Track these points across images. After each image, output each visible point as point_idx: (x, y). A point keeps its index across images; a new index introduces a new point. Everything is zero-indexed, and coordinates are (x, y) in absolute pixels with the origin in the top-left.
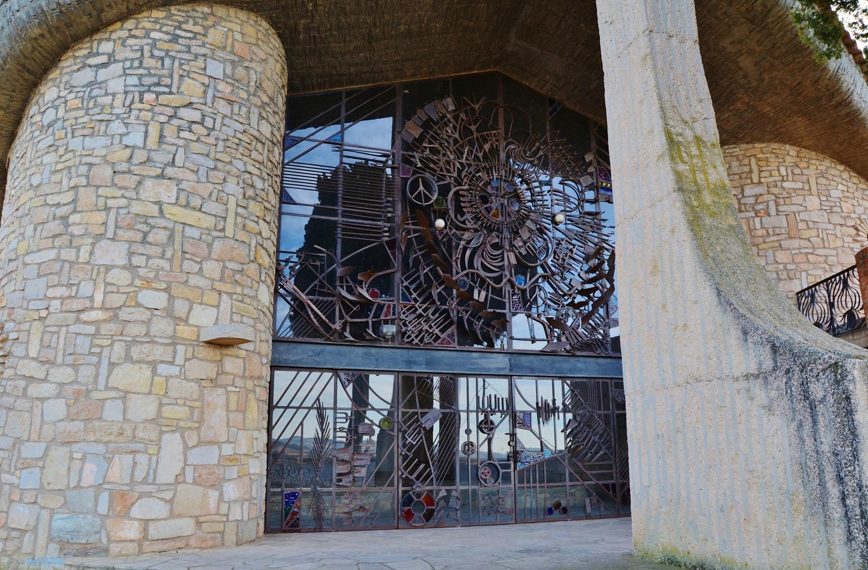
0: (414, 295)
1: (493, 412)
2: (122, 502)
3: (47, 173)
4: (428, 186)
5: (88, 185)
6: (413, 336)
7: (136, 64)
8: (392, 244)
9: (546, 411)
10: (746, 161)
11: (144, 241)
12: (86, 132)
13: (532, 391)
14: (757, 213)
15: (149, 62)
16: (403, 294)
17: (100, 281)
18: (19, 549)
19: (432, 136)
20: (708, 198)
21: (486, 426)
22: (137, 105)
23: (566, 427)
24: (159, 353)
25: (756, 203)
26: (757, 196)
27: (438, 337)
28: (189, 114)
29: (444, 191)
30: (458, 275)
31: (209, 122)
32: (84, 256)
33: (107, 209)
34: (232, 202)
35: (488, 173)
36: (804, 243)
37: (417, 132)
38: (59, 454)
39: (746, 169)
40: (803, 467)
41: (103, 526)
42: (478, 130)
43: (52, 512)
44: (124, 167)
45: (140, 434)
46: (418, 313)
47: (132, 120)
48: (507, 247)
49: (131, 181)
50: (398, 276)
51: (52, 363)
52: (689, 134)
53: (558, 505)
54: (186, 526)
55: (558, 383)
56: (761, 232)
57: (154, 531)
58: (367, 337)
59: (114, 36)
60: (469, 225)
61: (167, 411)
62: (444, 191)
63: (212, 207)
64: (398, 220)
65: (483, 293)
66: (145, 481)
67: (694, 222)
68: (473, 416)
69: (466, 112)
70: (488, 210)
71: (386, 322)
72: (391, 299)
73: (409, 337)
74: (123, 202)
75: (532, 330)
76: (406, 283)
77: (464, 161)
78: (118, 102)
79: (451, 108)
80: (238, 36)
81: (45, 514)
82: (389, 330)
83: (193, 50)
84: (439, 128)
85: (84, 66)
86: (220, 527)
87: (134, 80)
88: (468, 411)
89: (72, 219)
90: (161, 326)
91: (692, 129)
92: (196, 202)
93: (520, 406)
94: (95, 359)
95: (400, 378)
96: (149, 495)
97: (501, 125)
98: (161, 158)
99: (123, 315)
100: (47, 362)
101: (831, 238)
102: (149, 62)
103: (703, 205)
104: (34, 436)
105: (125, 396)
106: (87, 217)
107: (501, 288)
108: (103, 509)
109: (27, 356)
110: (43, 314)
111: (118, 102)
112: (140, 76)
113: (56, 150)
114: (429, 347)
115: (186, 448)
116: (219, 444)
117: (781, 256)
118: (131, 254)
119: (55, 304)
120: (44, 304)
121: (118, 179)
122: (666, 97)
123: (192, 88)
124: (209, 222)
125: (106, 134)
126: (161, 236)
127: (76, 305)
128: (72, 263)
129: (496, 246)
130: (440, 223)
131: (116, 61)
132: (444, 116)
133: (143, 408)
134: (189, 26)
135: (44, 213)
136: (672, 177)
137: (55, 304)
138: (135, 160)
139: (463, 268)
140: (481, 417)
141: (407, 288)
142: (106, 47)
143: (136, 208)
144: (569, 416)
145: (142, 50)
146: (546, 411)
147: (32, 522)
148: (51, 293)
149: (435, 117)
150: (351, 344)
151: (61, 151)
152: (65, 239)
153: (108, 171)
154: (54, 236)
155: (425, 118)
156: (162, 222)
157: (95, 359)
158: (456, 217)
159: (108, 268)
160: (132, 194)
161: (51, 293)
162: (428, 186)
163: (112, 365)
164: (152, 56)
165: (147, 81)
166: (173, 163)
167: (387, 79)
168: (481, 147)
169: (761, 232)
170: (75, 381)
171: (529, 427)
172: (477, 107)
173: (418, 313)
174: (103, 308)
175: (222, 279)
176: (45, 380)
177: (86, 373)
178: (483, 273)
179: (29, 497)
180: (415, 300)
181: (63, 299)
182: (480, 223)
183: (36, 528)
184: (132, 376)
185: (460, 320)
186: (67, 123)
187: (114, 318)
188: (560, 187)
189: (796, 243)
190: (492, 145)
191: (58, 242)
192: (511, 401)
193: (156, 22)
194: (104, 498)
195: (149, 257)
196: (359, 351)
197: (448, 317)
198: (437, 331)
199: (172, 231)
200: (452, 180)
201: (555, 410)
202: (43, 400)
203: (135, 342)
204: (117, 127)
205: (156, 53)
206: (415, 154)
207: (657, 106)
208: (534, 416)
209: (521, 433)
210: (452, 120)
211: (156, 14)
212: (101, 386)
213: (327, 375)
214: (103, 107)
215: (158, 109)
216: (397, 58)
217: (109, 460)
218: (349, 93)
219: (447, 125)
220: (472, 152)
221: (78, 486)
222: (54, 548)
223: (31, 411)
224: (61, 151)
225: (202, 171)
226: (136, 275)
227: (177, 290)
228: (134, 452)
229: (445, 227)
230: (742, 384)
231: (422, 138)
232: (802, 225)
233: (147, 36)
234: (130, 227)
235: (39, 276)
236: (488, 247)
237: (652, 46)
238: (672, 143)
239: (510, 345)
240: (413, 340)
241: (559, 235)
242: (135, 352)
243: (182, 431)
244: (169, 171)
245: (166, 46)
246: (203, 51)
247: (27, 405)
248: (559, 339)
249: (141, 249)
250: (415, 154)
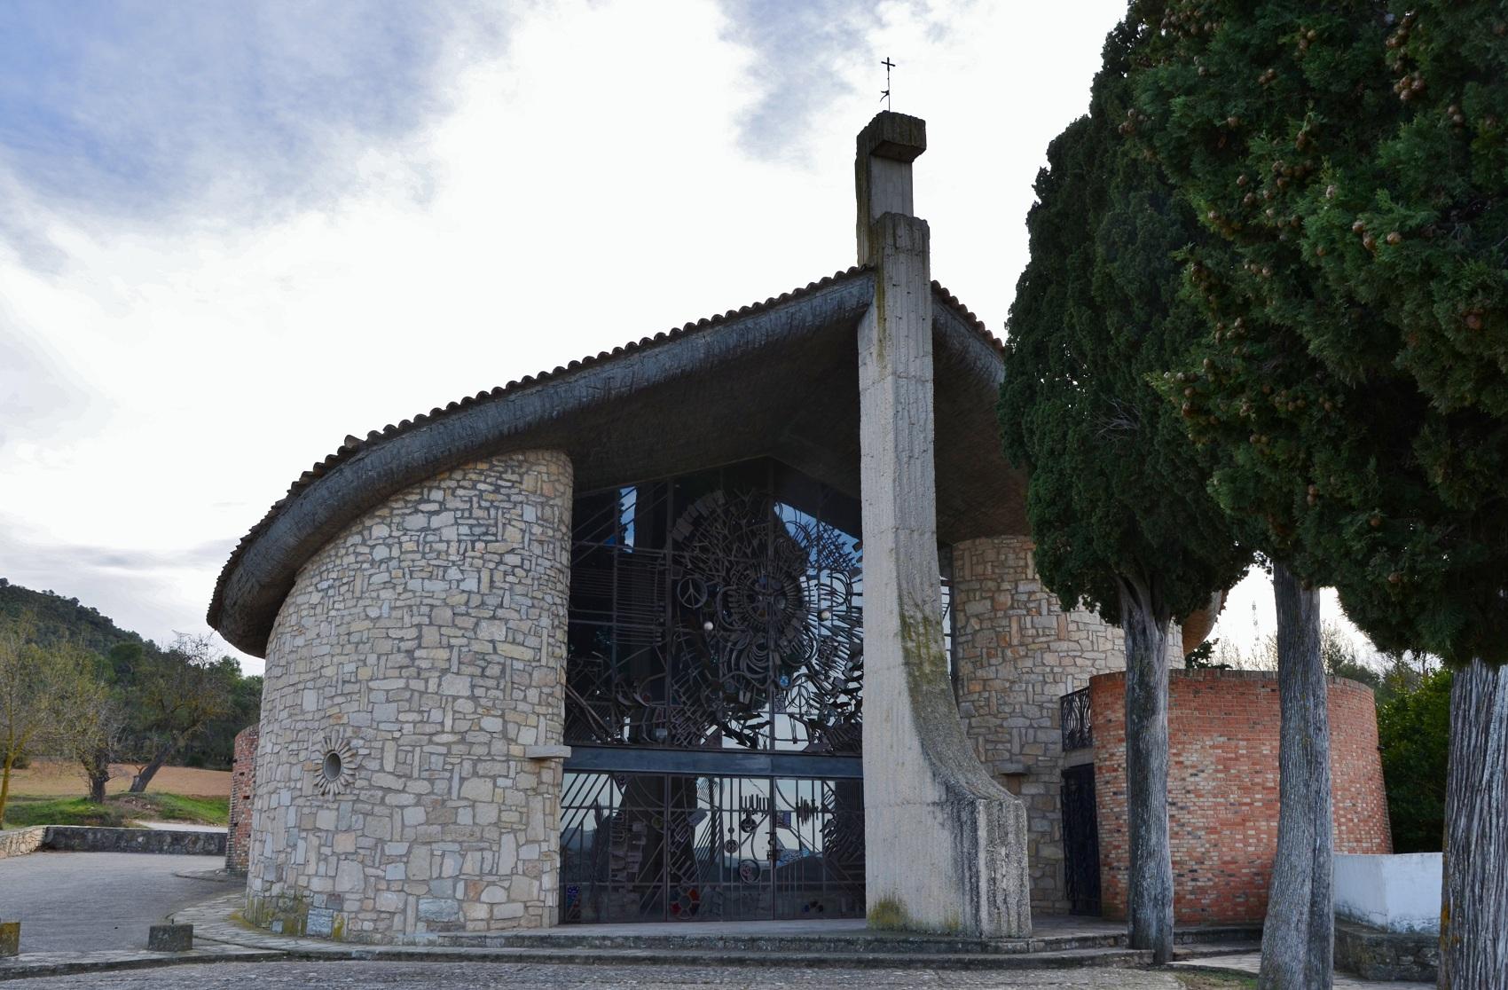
1: (755, 812)
2: (474, 888)
3: (386, 608)
4: (697, 588)
5: (431, 624)
7: (466, 514)
8: (663, 649)
9: (805, 811)
10: (1022, 555)
11: (483, 675)
12: (424, 575)
13: (792, 791)
14: (1029, 610)
15: (477, 513)
17: (449, 708)
18: (389, 928)
20: (927, 668)
21: (748, 825)
22: (470, 553)
23: (824, 827)
24: (498, 768)
25: (1029, 601)
26: (1031, 593)
28: (512, 560)
29: (712, 594)
31: (527, 566)
32: (432, 687)
33: (451, 647)
34: (545, 637)
36: (1073, 645)
38: (421, 852)
39: (1022, 563)
40: (956, 861)
41: (460, 908)
43: (418, 897)
44: (463, 609)
45: (487, 835)
47: (466, 567)
49: (469, 623)
50: (668, 680)
51: (410, 777)
52: (919, 616)
53: (814, 904)
54: (518, 909)
55: (818, 783)
56: (1031, 632)
57: (497, 912)
59: (443, 485)
61: (505, 816)
62: (712, 594)
63: (532, 641)
64: (669, 623)
65: (748, 695)
66: (490, 873)
67: (914, 690)
68: (736, 815)
71: (658, 726)
74: (464, 641)
75: (794, 730)
78: (453, 550)
79: (722, 501)
80: (545, 477)
81: (412, 899)
82: (662, 733)
83: (513, 498)
85: (417, 511)
86: (540, 911)
87: (464, 530)
88: (731, 811)
89: (417, 653)
90: (499, 746)
91: (922, 611)
92: (520, 638)
93: (781, 805)
94: (447, 775)
96: (494, 884)
98: (492, 601)
99: (469, 738)
100: (404, 776)
101: (1101, 640)
102: (477, 513)
103: (923, 675)
104: (397, 837)
105: (473, 805)
106: (433, 653)
108: (460, 895)
109: (382, 770)
110: (397, 735)
111: (453, 550)
112: (471, 526)
113: (394, 588)
115: (518, 846)
116: (538, 842)
117: (1050, 658)
118: (473, 687)
119: (408, 728)
120: (397, 726)
121: (459, 621)
122: (904, 586)
123: (513, 534)
124: (529, 654)
125: (443, 578)
126: (494, 670)
127: (428, 729)
128: (422, 693)
129: (761, 647)
130: (709, 626)
131: (447, 510)
132: (713, 512)
133: (488, 814)
134: (508, 476)
135: (386, 646)
136: (901, 653)
137: (408, 728)
138: (472, 604)
140: (744, 817)
142: (437, 495)
143: (476, 647)
144: (829, 816)
145: (471, 501)
146: (805, 811)
147: (401, 906)
148: (402, 717)
149: (705, 513)
151: (400, 589)
152: (413, 671)
153: (449, 613)
154: (401, 668)
155: (695, 514)
156: (496, 658)
157: (447, 775)
159: (455, 698)
160: (471, 634)
161: (402, 717)
162: (697, 588)
163: (462, 780)
164: (480, 507)
165: (477, 530)
166: (501, 606)
168: (750, 543)
169: (1031, 632)
170: (432, 793)
171: (788, 827)
174: (453, 732)
175: (540, 704)
176: (403, 791)
177: (441, 786)
178: (748, 675)
179: (395, 886)
181: (415, 723)
183: (404, 911)
184: (478, 789)
186: (404, 564)
187: (463, 741)
188: (828, 582)
189: (1064, 645)
191: (405, 673)
192: (772, 800)
193: (481, 473)
194: (461, 886)
195: (488, 689)
196: (633, 753)
199: (504, 665)
201: (814, 810)
202: (402, 807)
203: (479, 760)
204: (453, 573)
205: (483, 504)
207: (895, 594)
208: (794, 815)
209: (782, 833)
211: (481, 466)
212: (454, 796)
213: (604, 777)
214: (439, 553)
215: (487, 557)
217: (464, 856)
221: (440, 877)
222: (421, 925)
223: (391, 816)
224: (400, 589)
225: (523, 610)
226: (477, 705)
227: (510, 716)
228: (482, 850)
230: (931, 808)
231: (692, 535)
232: (1072, 627)
233: (474, 488)
234: (471, 664)
235: (388, 701)
237: (897, 542)
238: (906, 626)
239: (772, 745)
241: (825, 632)
242: (481, 768)
243: (514, 831)
244: (500, 612)
245: (491, 497)
246: (520, 498)
247: (387, 812)
248: (820, 738)
249: (481, 682)
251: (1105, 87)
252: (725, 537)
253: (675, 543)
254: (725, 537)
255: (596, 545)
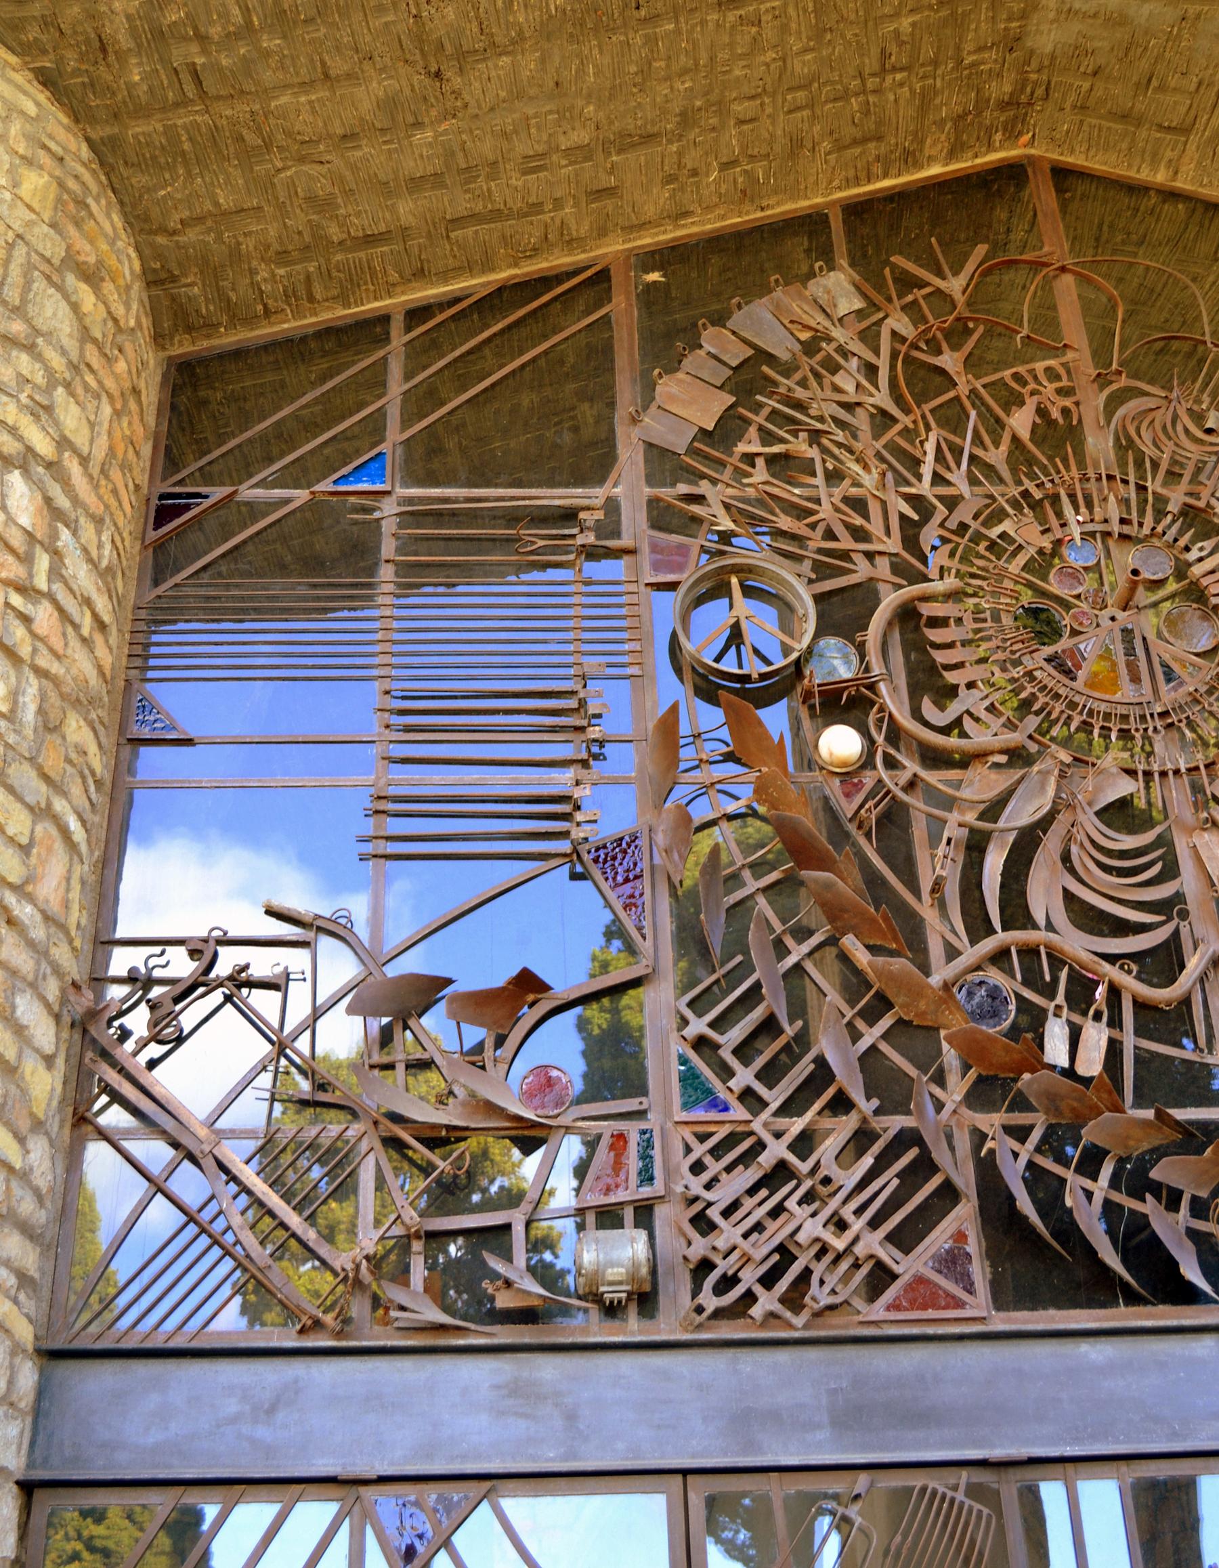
0: (744, 1077)
6: (749, 1277)
16: (690, 1079)
19: (774, 415)
27: (881, 1277)
30: (952, 955)
35: (1042, 519)
37: (707, 410)
42: (971, 364)
46: (766, 1160)
48: (1188, 814)
58: (504, 1301)
60: (980, 737)
65: (1096, 1037)
69: (911, 309)
70: (1064, 666)
72: (631, 1104)
73: (727, 1282)
76: (698, 1026)
77: (924, 487)
79: (850, 303)
84: (803, 383)
95: (697, 1502)
97: (1074, 330)
107: (1186, 1002)
114: (836, 1326)
139: (978, 927)
141: (701, 1043)
149: (782, 345)
150: (432, 1344)
155: (736, 354)
158: (917, 714)
167: (572, 243)
168: (996, 426)
172: (955, 285)
173: (766, 1160)
178: (1078, 945)
180: (747, 1096)
182: (1032, 722)
185: (987, 1169)
190: (1041, 412)
197: (925, 1166)
198: (873, 1244)
200: (883, 564)
206: (704, 487)
210: (856, 346)
213: (314, 1515)
216: (581, 136)
218: (416, 315)
219: (834, 369)
220: (957, 452)
229: (867, 761)
231: (725, 431)
236: (1090, 824)
240: (749, 1298)
250: (704, 487)
251: (913, 1289)
252: (883, 419)
253: (656, 454)
254: (883, 419)
255: (301, 496)
